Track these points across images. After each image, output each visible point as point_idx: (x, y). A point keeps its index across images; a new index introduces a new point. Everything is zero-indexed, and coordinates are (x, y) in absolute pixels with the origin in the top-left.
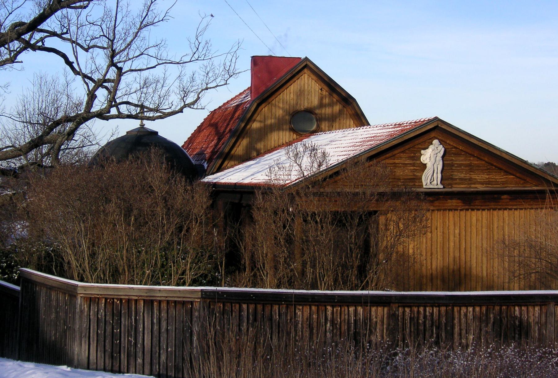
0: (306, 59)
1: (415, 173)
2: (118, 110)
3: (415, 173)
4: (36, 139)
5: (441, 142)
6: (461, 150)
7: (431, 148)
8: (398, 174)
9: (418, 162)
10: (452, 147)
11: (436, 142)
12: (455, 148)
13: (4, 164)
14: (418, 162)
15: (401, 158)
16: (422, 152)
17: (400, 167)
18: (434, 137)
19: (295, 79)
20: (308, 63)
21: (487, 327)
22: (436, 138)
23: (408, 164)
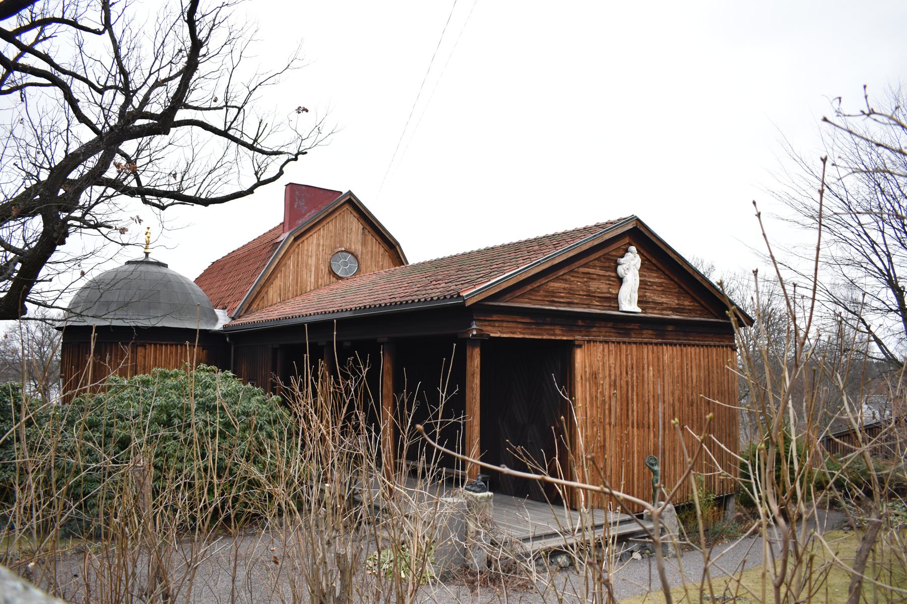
0: (350, 193)
3: (611, 290)
15: (595, 266)
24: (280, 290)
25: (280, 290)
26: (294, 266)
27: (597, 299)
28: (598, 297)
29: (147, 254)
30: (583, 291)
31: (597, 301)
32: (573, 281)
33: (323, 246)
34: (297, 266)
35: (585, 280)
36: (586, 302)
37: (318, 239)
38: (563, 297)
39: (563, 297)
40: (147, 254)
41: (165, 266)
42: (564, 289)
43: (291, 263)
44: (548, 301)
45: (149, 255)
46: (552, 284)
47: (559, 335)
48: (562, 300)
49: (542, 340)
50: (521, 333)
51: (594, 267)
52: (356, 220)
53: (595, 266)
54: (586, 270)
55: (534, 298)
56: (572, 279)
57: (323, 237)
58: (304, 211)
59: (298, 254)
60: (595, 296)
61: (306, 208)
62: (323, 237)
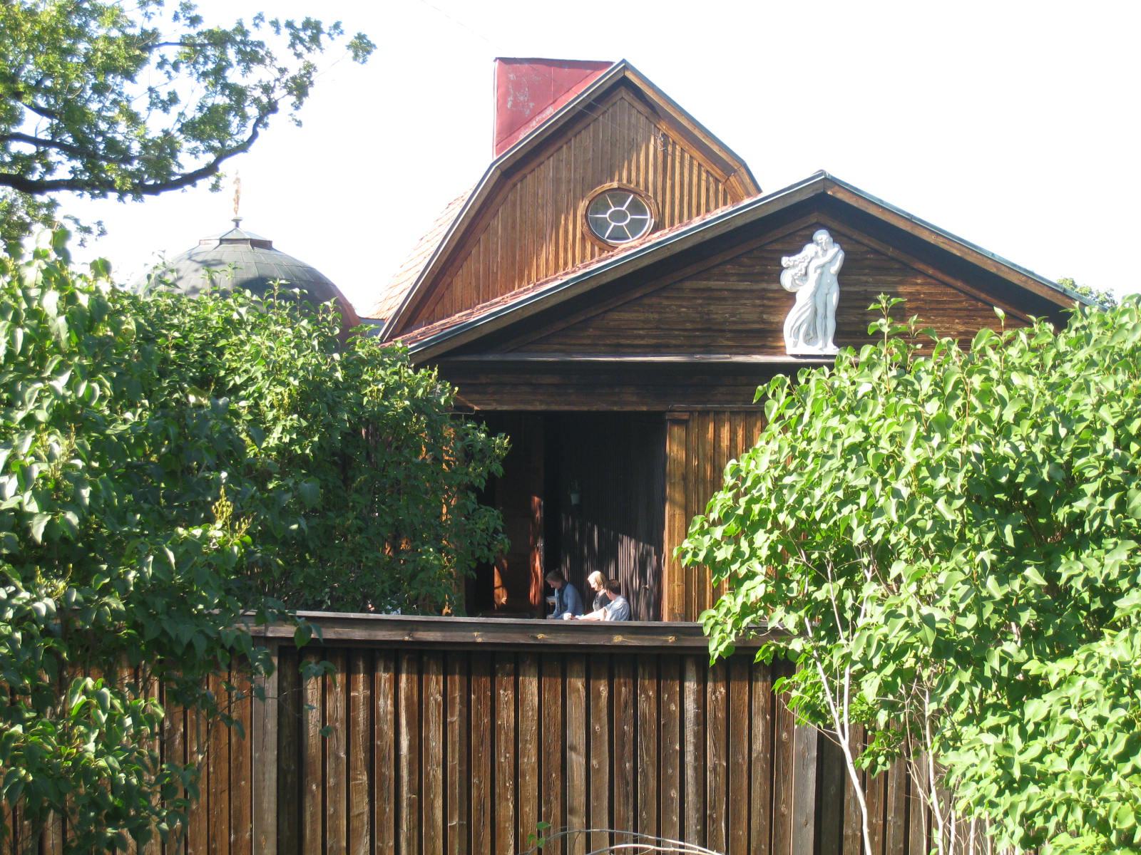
0: (626, 66)
1: (765, 316)
2: (13, 606)
3: (765, 316)
4: (241, 557)
5: (837, 237)
6: (892, 259)
7: (809, 249)
8: (718, 317)
9: (774, 287)
10: (865, 248)
11: (822, 236)
12: (876, 252)
13: (5, 171)
14: (774, 287)
15: (726, 275)
16: (785, 261)
17: (725, 299)
18: (817, 223)
19: (579, 127)
20: (629, 75)
21: (138, 124)
22: (821, 226)
23: (745, 291)
24: (478, 279)
25: (478, 279)
26: (504, 229)
27: (729, 335)
28: (730, 331)
29: (237, 222)
30: (693, 322)
31: (728, 339)
32: (669, 306)
33: (569, 182)
34: (514, 227)
35: (700, 301)
36: (701, 342)
37: (557, 169)
38: (642, 337)
39: (642, 337)
40: (237, 222)
41: (265, 245)
42: (646, 321)
43: (498, 224)
44: (605, 345)
45: (240, 223)
46: (616, 316)
47: (632, 402)
48: (642, 342)
49: (589, 412)
50: (541, 402)
51: (723, 277)
52: (642, 119)
53: (726, 275)
54: (703, 284)
55: (573, 342)
56: (665, 302)
57: (568, 163)
58: (528, 112)
59: (514, 204)
60: (723, 331)
61: (532, 105)
62: (568, 163)
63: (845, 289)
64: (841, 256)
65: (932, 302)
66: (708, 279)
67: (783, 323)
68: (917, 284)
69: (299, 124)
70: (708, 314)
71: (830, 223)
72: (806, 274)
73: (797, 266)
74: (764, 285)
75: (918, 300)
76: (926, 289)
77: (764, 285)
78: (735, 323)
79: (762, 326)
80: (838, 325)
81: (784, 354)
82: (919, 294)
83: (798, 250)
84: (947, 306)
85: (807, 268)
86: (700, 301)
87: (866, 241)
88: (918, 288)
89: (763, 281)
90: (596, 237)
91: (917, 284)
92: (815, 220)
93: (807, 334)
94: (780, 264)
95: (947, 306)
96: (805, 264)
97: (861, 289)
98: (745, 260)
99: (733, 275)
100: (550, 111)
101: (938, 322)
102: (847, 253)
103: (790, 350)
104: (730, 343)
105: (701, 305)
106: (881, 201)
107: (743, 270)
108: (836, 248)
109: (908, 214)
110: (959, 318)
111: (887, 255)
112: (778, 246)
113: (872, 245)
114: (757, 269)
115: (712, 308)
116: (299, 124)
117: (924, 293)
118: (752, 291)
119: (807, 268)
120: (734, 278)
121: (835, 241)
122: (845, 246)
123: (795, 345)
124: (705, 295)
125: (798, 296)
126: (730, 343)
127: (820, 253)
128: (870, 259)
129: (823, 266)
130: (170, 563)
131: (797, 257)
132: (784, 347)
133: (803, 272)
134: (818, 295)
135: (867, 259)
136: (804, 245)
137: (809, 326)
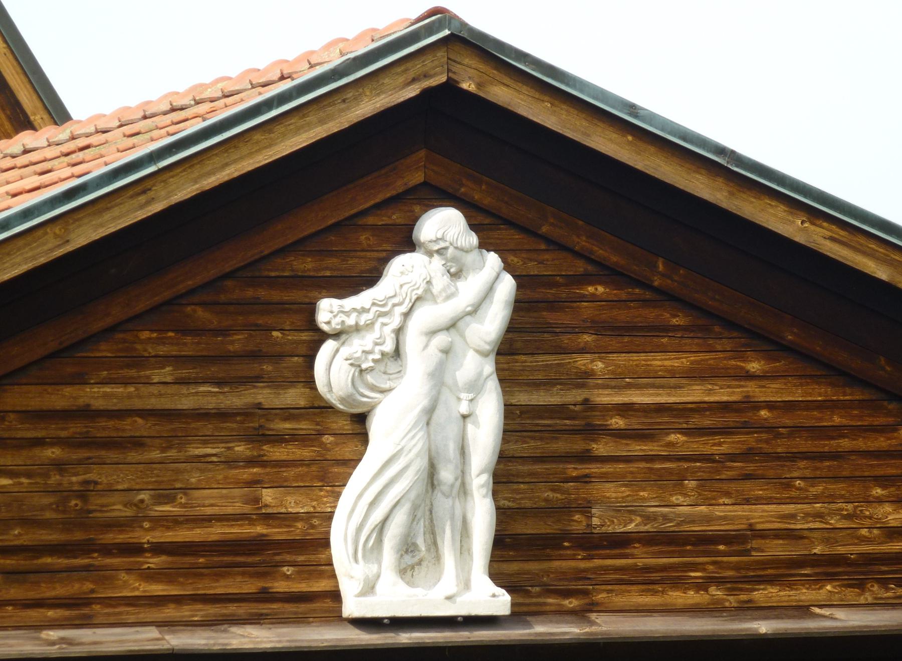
3: (268, 496)
9: (293, 397)
14: (293, 397)
17: (137, 443)
18: (425, 184)
27: (154, 562)
28: (158, 549)
31: (151, 576)
60: (136, 549)
63: (523, 398)
64: (507, 285)
65: (796, 430)
66: (80, 380)
67: (329, 517)
68: (750, 376)
69: (413, 267)
70: (83, 495)
71: (465, 190)
72: (397, 353)
73: (370, 326)
74: (264, 396)
75: (746, 427)
76: (774, 392)
77: (264, 396)
78: (174, 522)
79: (260, 529)
80: (503, 515)
81: (335, 617)
82: (757, 406)
83: (371, 279)
84: (845, 444)
85: (399, 332)
86: (52, 453)
87: (581, 242)
88: (752, 389)
89: (255, 380)
90: (728, 163)
91: (750, 376)
92: (417, 178)
93: (407, 547)
94: (311, 324)
95: (845, 444)
96: (395, 321)
97: (574, 396)
98: (201, 313)
99: (163, 360)
100: (747, 587)
101: (816, 499)
102: (522, 281)
103: (352, 607)
104: (157, 589)
105: (59, 466)
106: (632, 108)
107: (190, 346)
108: (493, 260)
109: (721, 150)
110: (883, 481)
111: (649, 287)
112: (306, 265)
113: (600, 252)
114: (237, 342)
115: (100, 475)
116: (413, 267)
117: (770, 406)
118: (223, 415)
119: (399, 332)
120: (167, 373)
121: (485, 245)
122: (512, 258)
123: (369, 589)
124: (74, 429)
125: (376, 427)
126: (157, 589)
127: (441, 281)
128: (593, 298)
129: (452, 326)
130: (441, 17)
131: (365, 298)
132: (335, 596)
133: (389, 347)
134: (440, 414)
135: (582, 298)
136: (385, 261)
137: (413, 517)
